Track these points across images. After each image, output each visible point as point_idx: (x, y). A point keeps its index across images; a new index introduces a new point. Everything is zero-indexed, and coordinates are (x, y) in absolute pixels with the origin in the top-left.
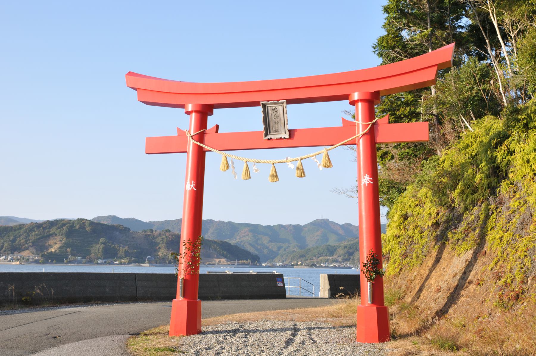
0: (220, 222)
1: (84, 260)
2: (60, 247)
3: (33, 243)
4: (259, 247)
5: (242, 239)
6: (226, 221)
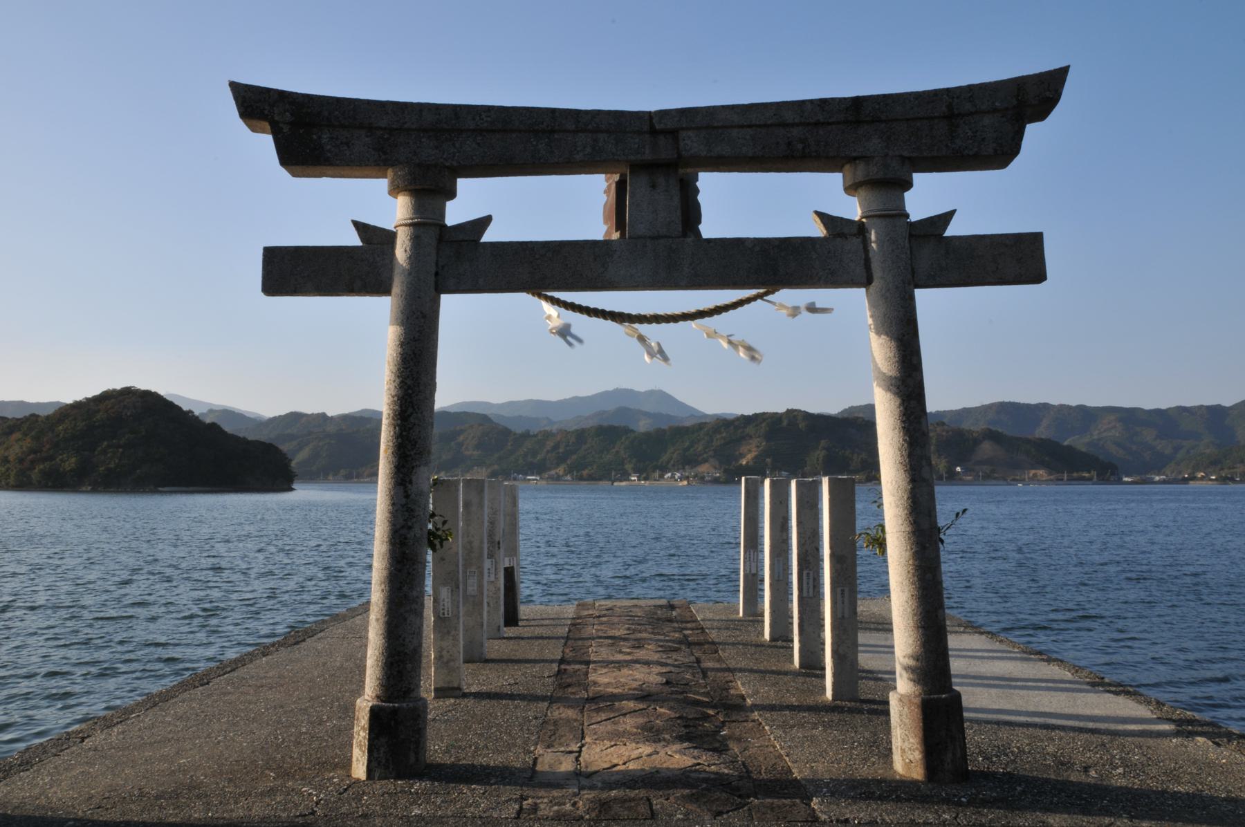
0: (1061, 406)
2: (756, 457)
4: (1134, 448)
5: (1105, 434)
6: (1074, 403)
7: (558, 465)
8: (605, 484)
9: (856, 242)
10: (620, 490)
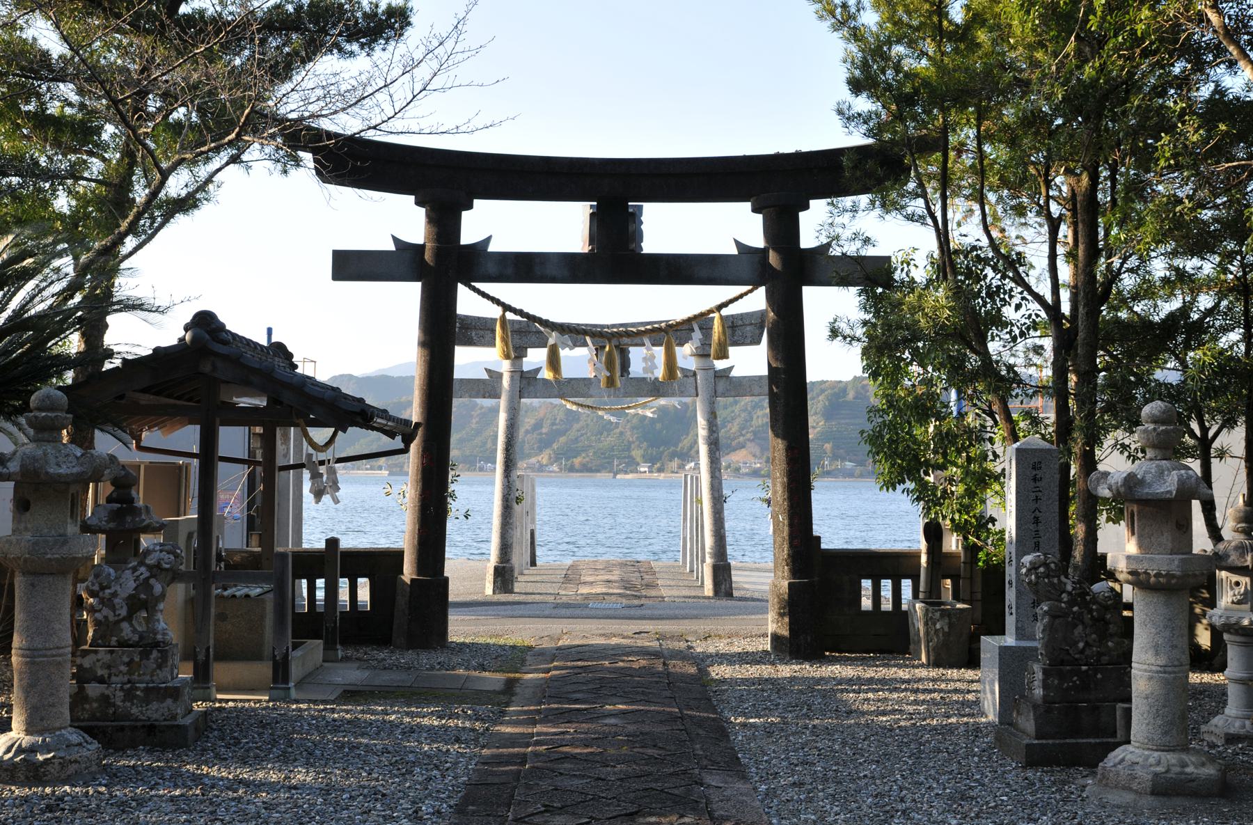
1: (858, 470)
3: (755, 433)
7: (541, 450)
8: (604, 476)
9: (692, 379)
10: (629, 484)
